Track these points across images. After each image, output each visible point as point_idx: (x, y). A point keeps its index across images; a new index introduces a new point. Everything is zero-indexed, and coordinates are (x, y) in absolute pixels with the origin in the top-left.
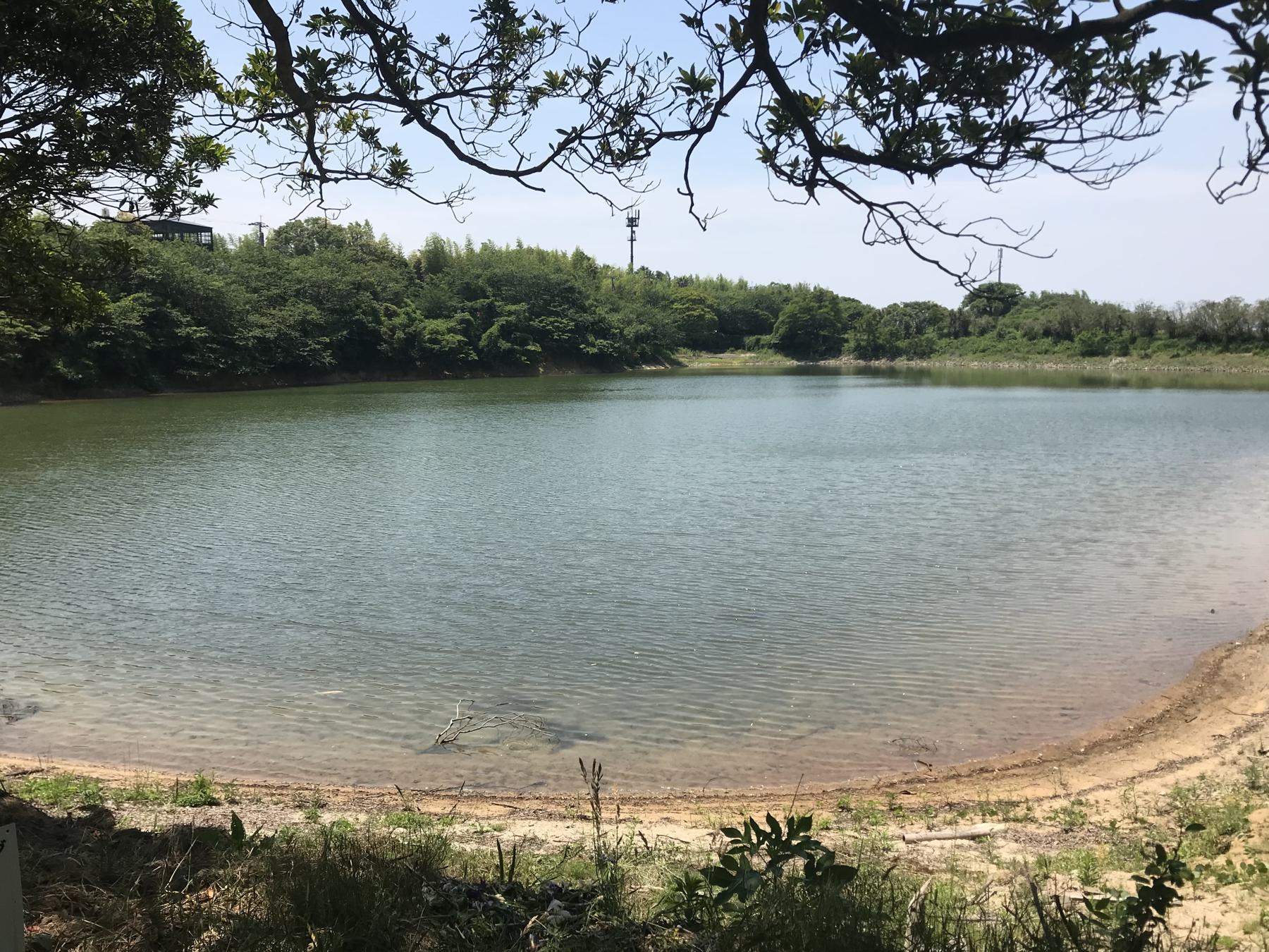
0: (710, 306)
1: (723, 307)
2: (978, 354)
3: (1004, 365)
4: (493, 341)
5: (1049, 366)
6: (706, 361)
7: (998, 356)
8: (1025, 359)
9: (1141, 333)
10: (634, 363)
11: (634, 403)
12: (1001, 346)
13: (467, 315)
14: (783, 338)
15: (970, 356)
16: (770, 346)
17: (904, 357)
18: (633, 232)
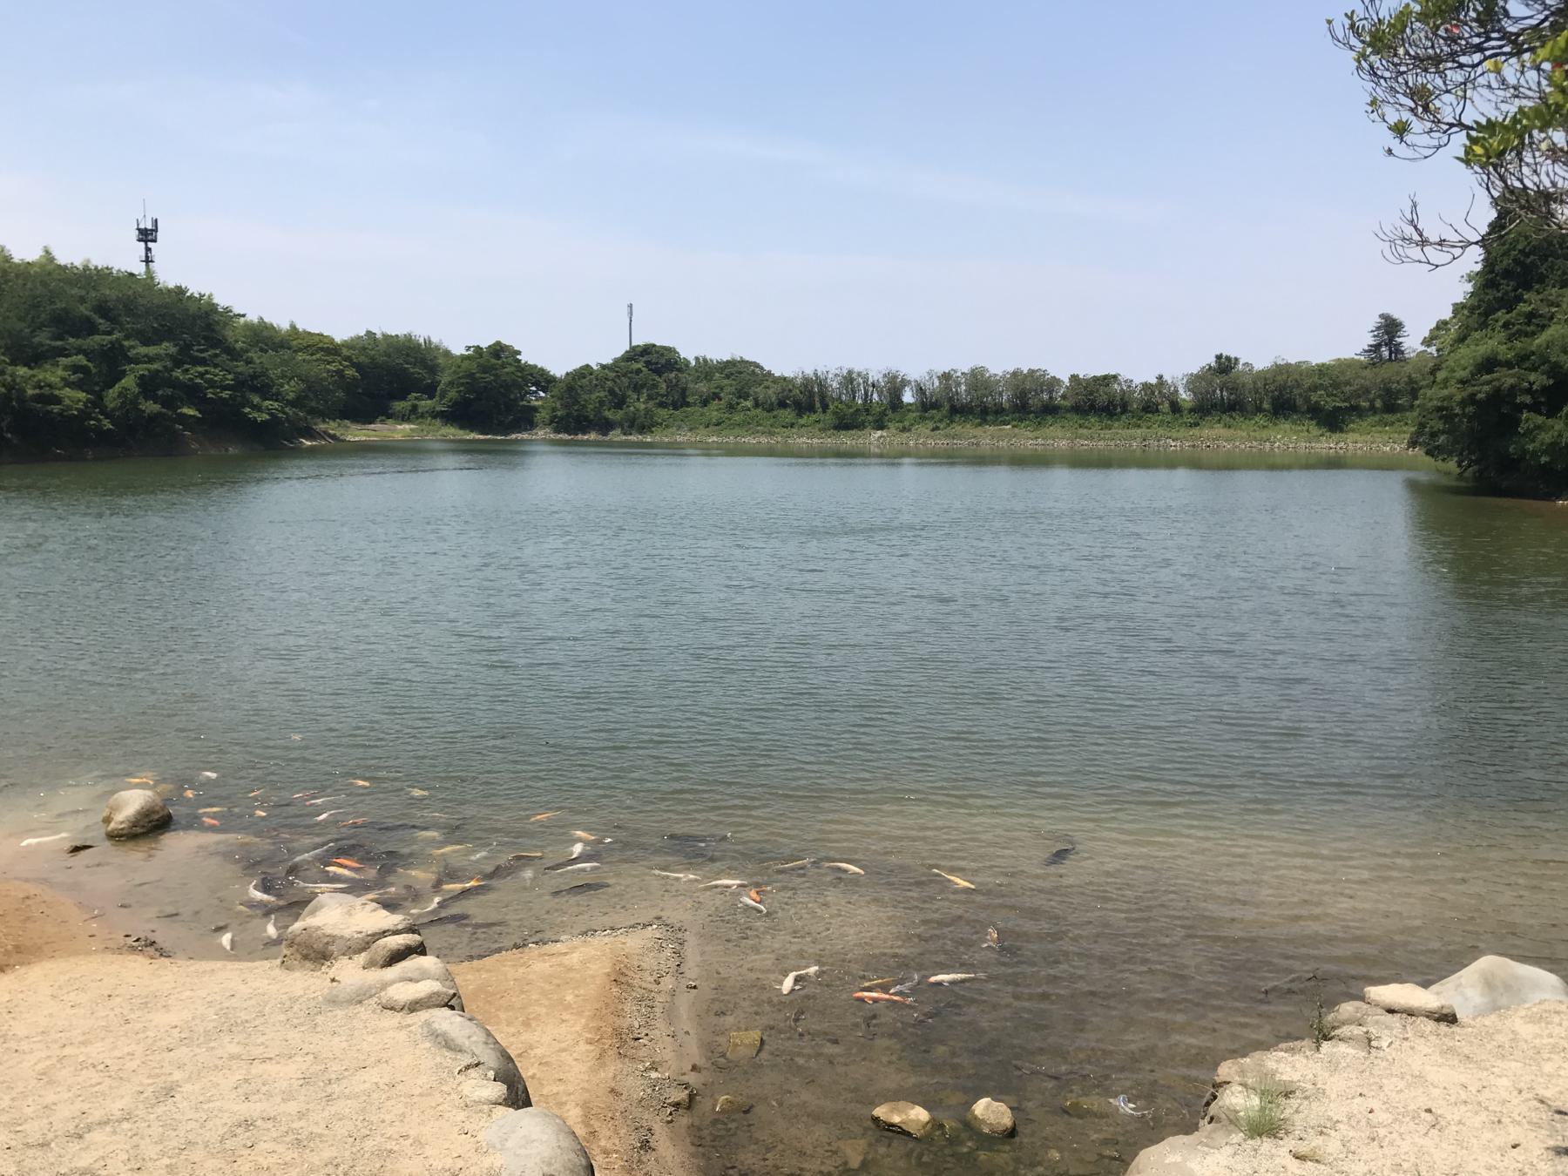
0: (348, 358)
1: (362, 359)
2: (712, 428)
3: (751, 440)
4: (129, 403)
5: (802, 441)
6: (357, 434)
7: (737, 431)
8: (771, 434)
9: (1152, 405)
10: (606, 426)
11: (1285, 473)
12: (737, 418)
13: (81, 359)
14: (455, 404)
15: (702, 430)
16: (435, 415)
17: (619, 431)
18: (148, 250)
